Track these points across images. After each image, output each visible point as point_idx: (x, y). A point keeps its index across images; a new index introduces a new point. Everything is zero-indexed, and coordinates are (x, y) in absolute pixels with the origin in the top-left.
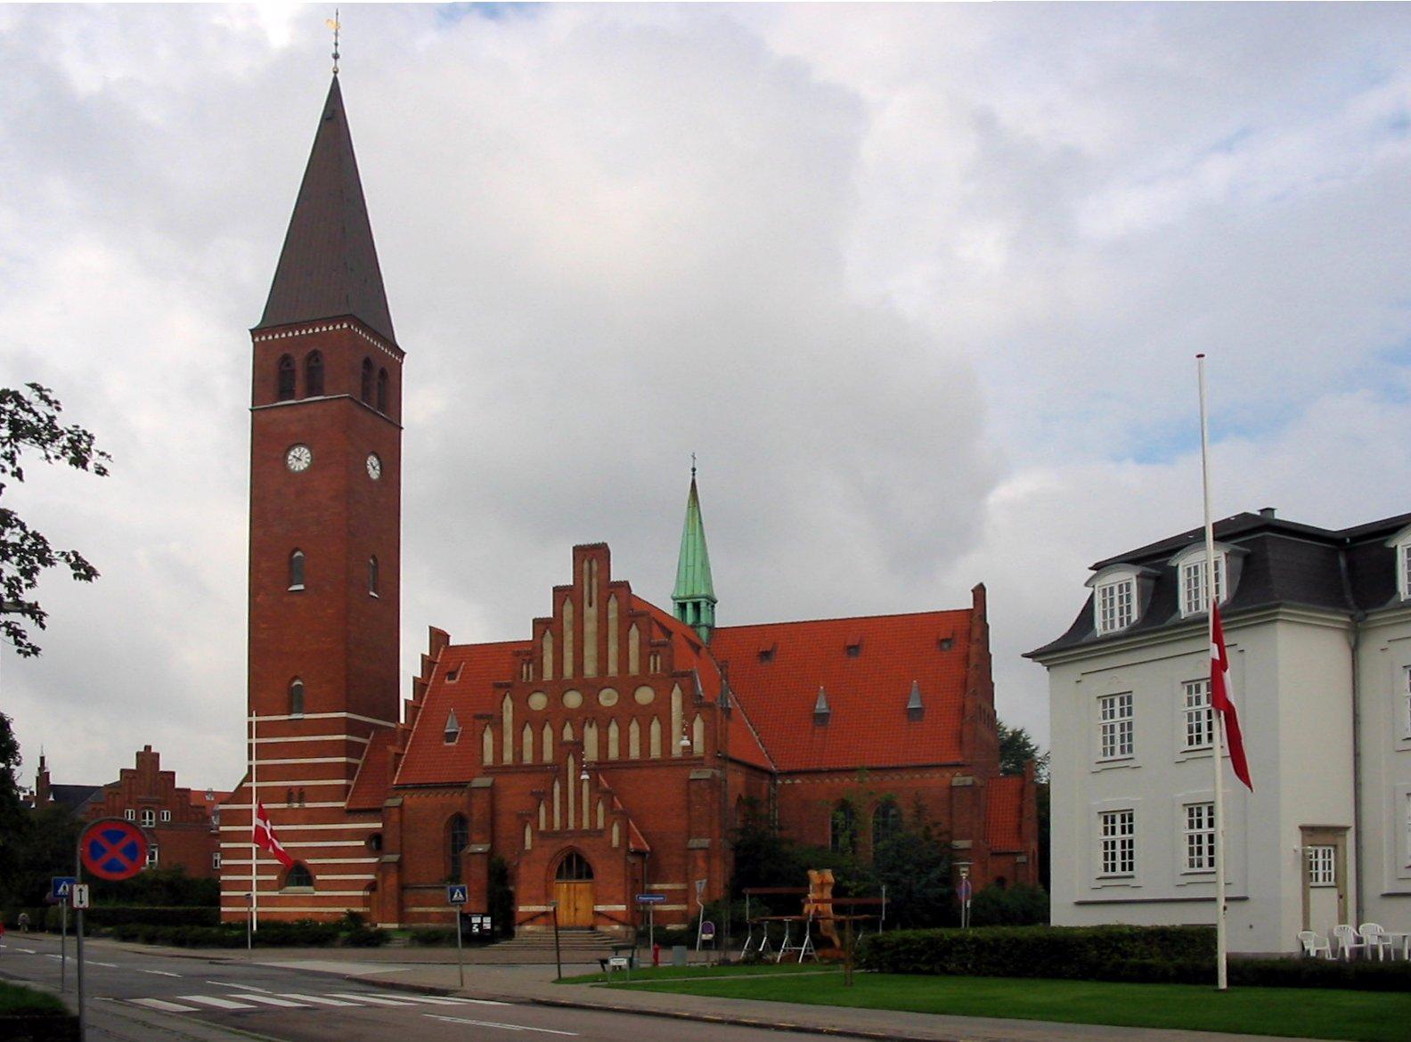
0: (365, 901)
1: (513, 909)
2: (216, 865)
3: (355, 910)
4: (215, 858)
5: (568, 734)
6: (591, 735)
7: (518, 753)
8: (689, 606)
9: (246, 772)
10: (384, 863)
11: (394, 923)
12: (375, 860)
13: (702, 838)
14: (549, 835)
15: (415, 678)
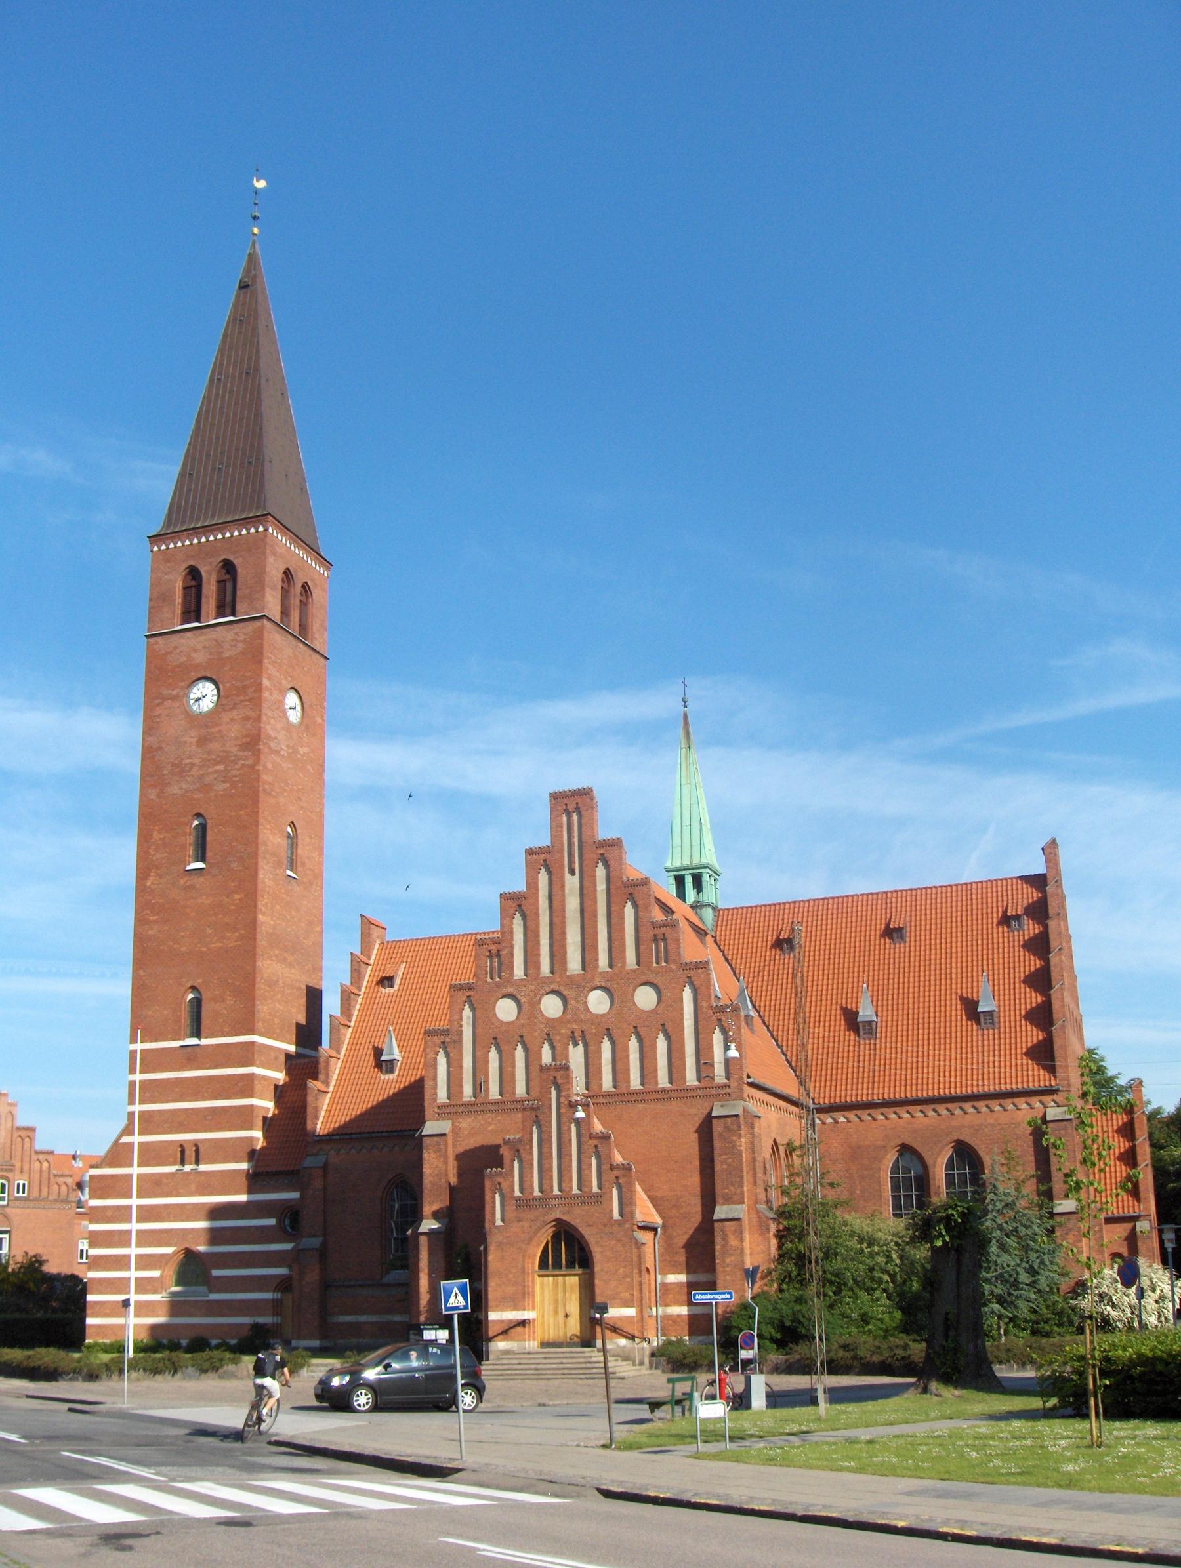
0: (276, 1307)
1: (482, 1317)
2: (82, 1257)
3: (261, 1320)
4: (80, 1247)
5: (546, 1056)
6: (576, 1056)
7: (479, 1086)
8: (689, 881)
9: (126, 1122)
10: (299, 1250)
11: (315, 1339)
12: (288, 1246)
13: (733, 1203)
14: (524, 1204)
15: (298, 1025)
